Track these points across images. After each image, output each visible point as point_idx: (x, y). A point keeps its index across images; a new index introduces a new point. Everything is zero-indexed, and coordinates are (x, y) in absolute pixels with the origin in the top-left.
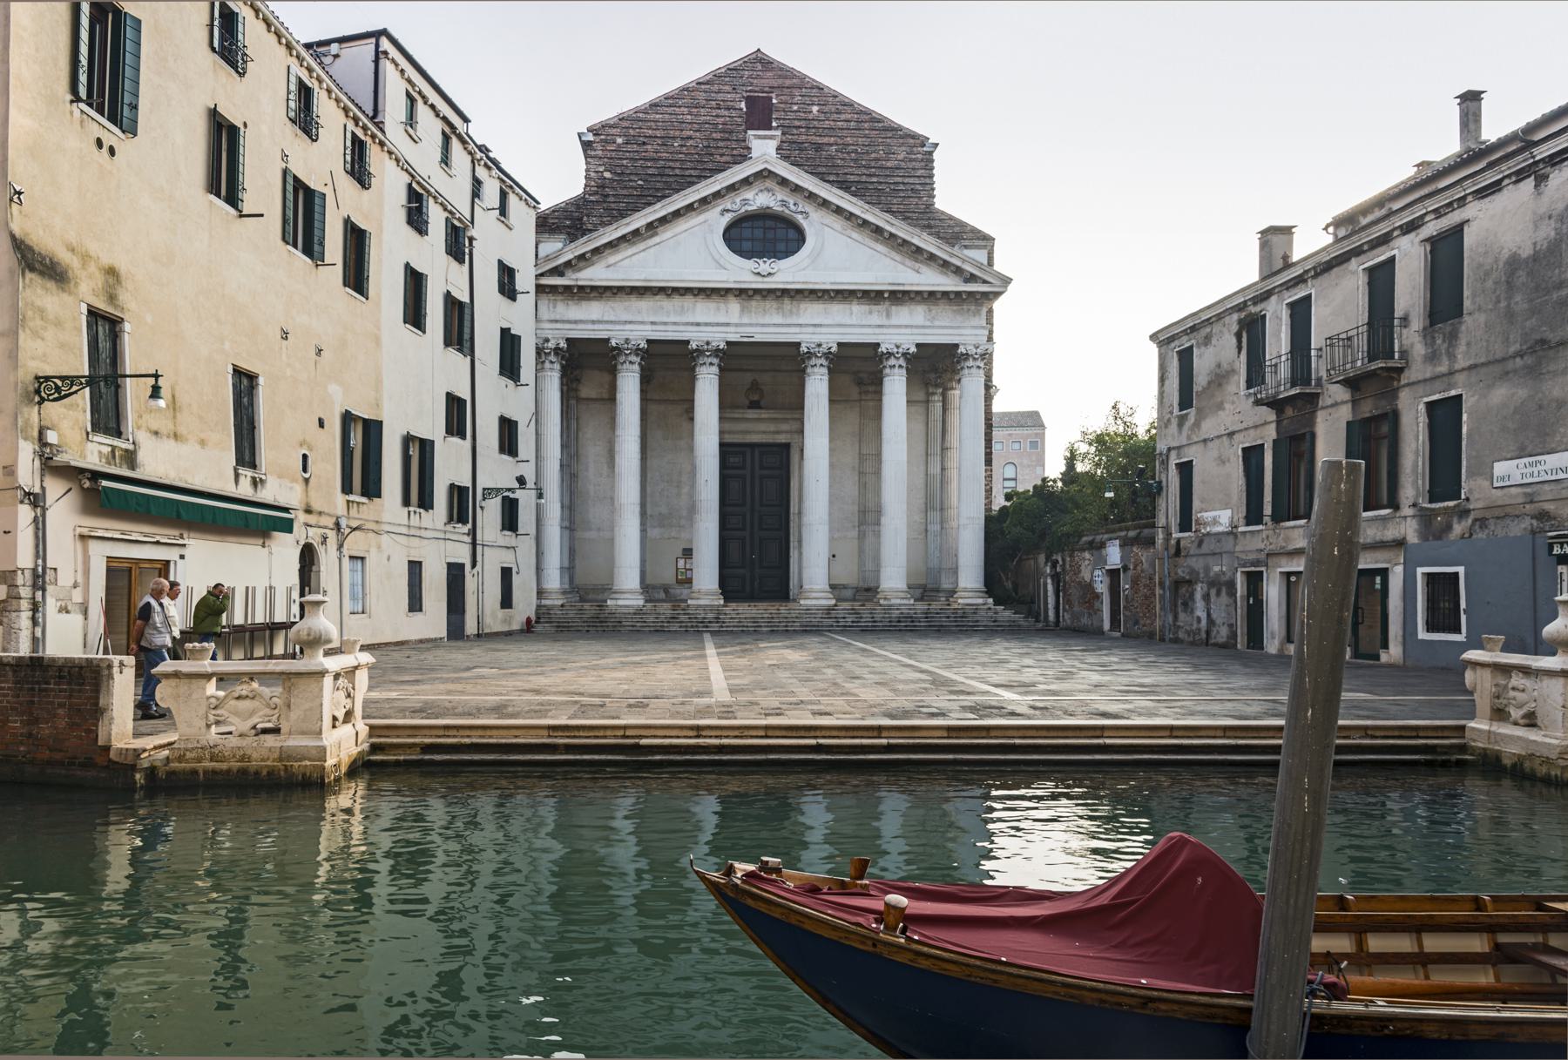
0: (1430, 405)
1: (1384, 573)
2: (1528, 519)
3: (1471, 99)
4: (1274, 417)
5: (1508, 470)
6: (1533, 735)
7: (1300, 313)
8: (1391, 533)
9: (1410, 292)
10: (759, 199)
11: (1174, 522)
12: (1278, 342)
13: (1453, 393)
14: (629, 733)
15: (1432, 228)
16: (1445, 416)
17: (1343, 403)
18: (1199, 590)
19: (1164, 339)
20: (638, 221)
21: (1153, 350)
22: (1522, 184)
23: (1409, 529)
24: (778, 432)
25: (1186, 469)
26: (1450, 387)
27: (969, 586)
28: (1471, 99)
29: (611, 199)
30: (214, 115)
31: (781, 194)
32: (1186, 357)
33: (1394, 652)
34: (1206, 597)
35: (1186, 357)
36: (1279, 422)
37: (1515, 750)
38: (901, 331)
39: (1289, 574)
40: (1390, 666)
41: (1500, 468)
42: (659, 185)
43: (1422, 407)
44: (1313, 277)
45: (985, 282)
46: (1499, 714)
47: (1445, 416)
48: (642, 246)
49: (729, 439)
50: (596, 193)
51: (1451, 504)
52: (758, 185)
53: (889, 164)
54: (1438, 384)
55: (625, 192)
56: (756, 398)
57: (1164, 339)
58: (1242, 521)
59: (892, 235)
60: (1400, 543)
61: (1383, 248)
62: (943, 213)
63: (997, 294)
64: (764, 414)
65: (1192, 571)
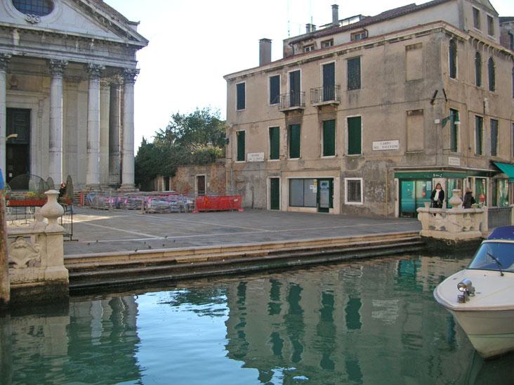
0: (348, 119)
1: (331, 180)
2: (384, 162)
3: (335, 7)
5: (378, 145)
6: (472, 233)
7: (295, 78)
8: (333, 165)
9: (341, 75)
11: (235, 156)
12: (285, 89)
13: (358, 115)
14: (165, 255)
15: (349, 55)
16: (354, 124)
18: (248, 186)
19: (230, 79)
21: (224, 82)
22: (380, 47)
23: (342, 164)
24: (25, 103)
25: (241, 136)
26: (358, 113)
27: (128, 182)
28: (335, 7)
30: (139, 23)
32: (241, 88)
33: (336, 210)
34: (252, 188)
35: (241, 88)
36: (286, 119)
38: (101, 60)
39: (290, 179)
40: (333, 215)
41: (375, 144)
43: (346, 119)
45: (137, 41)
46: (432, 228)
47: (354, 124)
51: (357, 155)
54: (352, 111)
56: (15, 84)
57: (230, 79)
58: (269, 157)
60: (339, 169)
61: (330, 58)
62: (106, 4)
63: (140, 47)
64: (20, 93)
65: (245, 177)
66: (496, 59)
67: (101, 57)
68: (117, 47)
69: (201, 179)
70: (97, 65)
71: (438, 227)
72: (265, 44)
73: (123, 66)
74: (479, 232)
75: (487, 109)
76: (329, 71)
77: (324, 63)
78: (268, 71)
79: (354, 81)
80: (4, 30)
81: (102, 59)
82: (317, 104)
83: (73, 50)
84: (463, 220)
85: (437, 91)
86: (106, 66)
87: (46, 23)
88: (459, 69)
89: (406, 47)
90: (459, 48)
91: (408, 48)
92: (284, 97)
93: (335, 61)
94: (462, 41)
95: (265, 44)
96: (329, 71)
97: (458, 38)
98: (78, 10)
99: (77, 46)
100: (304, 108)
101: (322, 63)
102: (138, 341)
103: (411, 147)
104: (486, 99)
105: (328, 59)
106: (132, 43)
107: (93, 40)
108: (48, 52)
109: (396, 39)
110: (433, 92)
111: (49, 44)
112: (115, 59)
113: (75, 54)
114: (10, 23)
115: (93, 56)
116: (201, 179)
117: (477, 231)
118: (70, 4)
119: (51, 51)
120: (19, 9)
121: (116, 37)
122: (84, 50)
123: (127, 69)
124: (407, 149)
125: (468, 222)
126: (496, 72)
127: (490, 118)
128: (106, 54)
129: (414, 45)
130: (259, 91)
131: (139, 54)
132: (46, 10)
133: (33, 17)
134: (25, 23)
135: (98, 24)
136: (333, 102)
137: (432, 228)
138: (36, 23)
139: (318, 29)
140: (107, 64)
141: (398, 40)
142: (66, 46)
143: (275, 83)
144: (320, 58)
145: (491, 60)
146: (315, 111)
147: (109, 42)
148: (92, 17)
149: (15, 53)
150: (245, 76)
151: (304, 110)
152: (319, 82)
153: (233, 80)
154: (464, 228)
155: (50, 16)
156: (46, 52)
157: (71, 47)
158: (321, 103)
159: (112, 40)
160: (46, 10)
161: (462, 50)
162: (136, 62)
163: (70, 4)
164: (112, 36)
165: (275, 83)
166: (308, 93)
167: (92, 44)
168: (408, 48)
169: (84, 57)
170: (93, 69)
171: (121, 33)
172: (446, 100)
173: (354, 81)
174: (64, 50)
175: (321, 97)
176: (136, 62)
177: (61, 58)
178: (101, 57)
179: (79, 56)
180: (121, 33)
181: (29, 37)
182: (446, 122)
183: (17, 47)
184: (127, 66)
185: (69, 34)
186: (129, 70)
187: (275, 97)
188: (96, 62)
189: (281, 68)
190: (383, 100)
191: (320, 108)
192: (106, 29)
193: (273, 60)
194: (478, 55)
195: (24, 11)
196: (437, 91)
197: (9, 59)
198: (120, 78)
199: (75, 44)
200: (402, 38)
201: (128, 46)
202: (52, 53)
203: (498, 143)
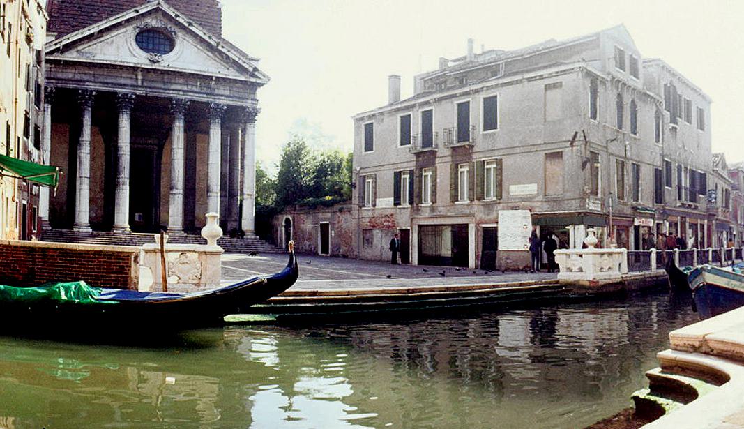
4: (415, 159)
6: (611, 273)
7: (427, 118)
10: (153, 22)
12: (416, 129)
17: (449, 156)
20: (94, 29)
21: (353, 122)
29: (65, 16)
31: (165, 21)
32: (369, 129)
35: (369, 129)
37: (123, 208)
38: (223, 98)
42: (89, 10)
44: (99, 68)
48: (95, 42)
49: (207, 136)
50: (57, 13)
52: (153, 16)
53: (201, 12)
55: (72, 12)
57: (359, 120)
59: (517, 81)
63: (261, 85)
66: (637, 101)
67: (222, 95)
68: (237, 85)
69: (325, 229)
70: (218, 105)
71: (575, 269)
72: (395, 79)
73: (244, 105)
74: (618, 273)
75: (629, 154)
76: (464, 110)
77: (459, 102)
78: (399, 110)
79: (490, 123)
80: (128, 70)
81: (223, 98)
82: (452, 146)
83: (194, 89)
84: (600, 260)
85: (576, 133)
86: (227, 105)
87: (169, 61)
88: (600, 110)
89: (546, 86)
90: (601, 89)
91: (547, 87)
92: (415, 138)
93: (470, 99)
94: (603, 82)
95: (395, 79)
96: (464, 110)
97: (599, 78)
98: (199, 46)
99: (199, 83)
100: (436, 150)
101: (456, 102)
102: (252, 421)
103: (551, 191)
104: (627, 143)
105: (465, 96)
106: (253, 80)
107: (214, 78)
108: (171, 92)
109: (535, 77)
110: (573, 134)
111: (171, 83)
112: (236, 98)
113: (196, 93)
114: (135, 63)
115: (213, 95)
116: (325, 229)
117: (616, 271)
118: (191, 41)
119: (173, 90)
120: (142, 48)
121: (237, 74)
122: (205, 89)
123: (248, 108)
124: (545, 193)
125: (606, 262)
126: (638, 115)
127: (631, 162)
128: (228, 93)
129: (554, 84)
130: (388, 130)
131: (259, 91)
132: (167, 48)
133: (156, 55)
134: (148, 62)
135: (219, 61)
136: (467, 143)
137: (570, 270)
138: (158, 62)
139: (451, 64)
140: (228, 102)
141: (538, 78)
142: (187, 85)
143: (406, 122)
144: (454, 96)
145: (633, 101)
146: (448, 152)
147: (230, 79)
148: (212, 53)
149: (138, 93)
150: (374, 115)
151: (436, 152)
152: (454, 124)
153: (362, 119)
154: (602, 268)
155: (171, 54)
156: (168, 92)
157: (192, 85)
158: (456, 144)
159: (234, 78)
160: (167, 48)
161: (603, 91)
162: (257, 101)
163: (191, 41)
164: (232, 74)
165: (406, 122)
166: (441, 132)
167: (213, 83)
168: (547, 87)
169: (205, 96)
170: (215, 109)
171: (242, 70)
172: (586, 142)
173: (490, 123)
174: (185, 88)
175: (455, 138)
176: (257, 101)
177: (183, 97)
178: (222, 95)
179: (201, 95)
180: (242, 70)
181: (151, 76)
182: (586, 165)
183: (140, 87)
184: (248, 105)
185: (189, 72)
186: (251, 109)
187: (405, 139)
188: (217, 101)
189: (413, 106)
190: (521, 142)
191: (454, 149)
192: (227, 66)
193: (402, 99)
194: (620, 96)
195: (147, 50)
196: (576, 133)
197: (133, 99)
198: (237, 120)
199: (197, 82)
200: (542, 76)
201: (249, 83)
202: (174, 92)
203: (640, 189)
